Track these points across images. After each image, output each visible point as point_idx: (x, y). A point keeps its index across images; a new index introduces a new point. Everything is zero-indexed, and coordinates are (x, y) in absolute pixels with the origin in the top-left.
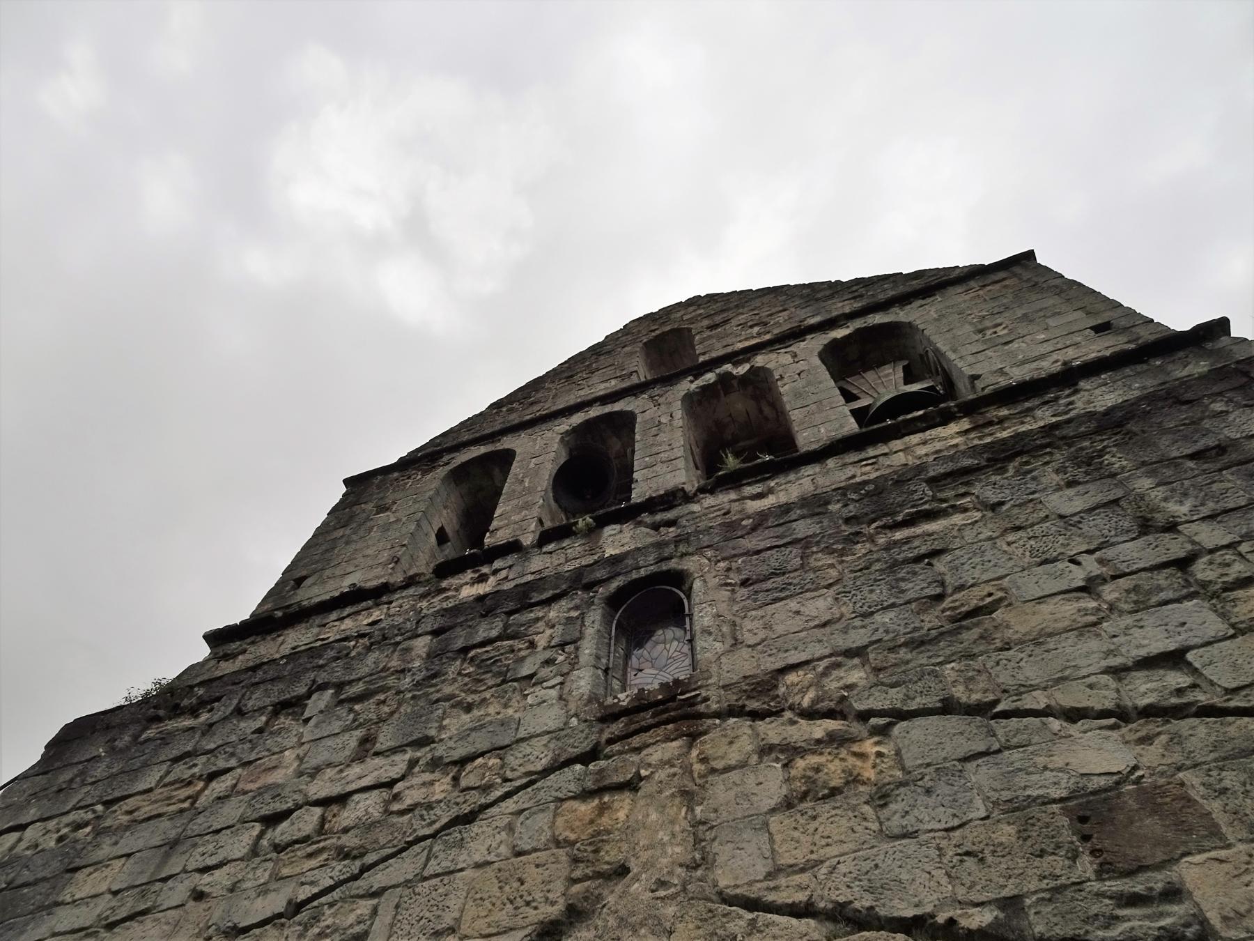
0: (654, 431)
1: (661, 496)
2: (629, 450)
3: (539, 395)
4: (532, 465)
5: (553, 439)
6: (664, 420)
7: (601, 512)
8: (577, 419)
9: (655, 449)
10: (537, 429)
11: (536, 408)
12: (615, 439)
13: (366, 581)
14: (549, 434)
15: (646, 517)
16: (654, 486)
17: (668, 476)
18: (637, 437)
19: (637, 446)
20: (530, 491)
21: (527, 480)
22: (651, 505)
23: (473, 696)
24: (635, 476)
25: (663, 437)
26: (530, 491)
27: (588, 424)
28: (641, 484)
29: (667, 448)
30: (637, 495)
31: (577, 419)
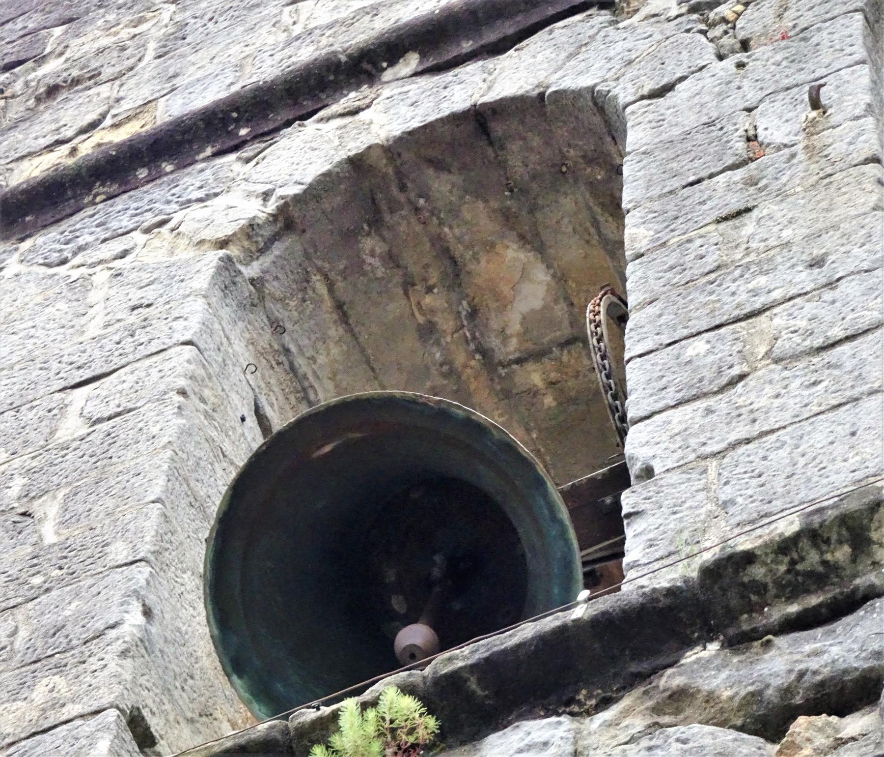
0: (725, 191)
1: (785, 546)
2: (596, 309)
3: (87, 43)
4: (71, 427)
5: (173, 275)
6: (779, 125)
7: (572, 534)
8: (304, 154)
9: (737, 294)
10: (84, 225)
11: (72, 112)
12: (513, 254)
13: (658, 84)
14: (151, 251)
15: (707, 667)
16: (746, 498)
17: (819, 435)
18: (636, 232)
19: (637, 282)
20: (71, 564)
21: (49, 510)
22: (724, 601)
23: (640, 669)
24: (638, 445)
25: (775, 222)
26: (71, 564)
27: (366, 187)
28: (672, 486)
29: (805, 279)
30: (657, 554)
31: (304, 154)
